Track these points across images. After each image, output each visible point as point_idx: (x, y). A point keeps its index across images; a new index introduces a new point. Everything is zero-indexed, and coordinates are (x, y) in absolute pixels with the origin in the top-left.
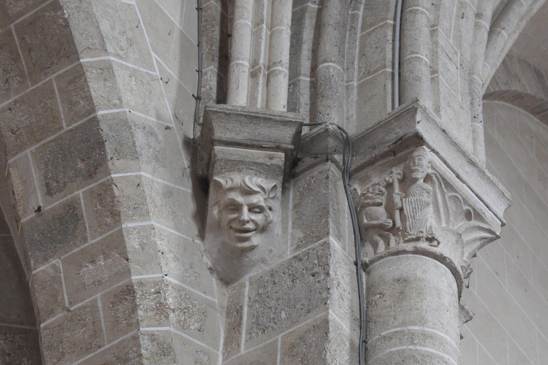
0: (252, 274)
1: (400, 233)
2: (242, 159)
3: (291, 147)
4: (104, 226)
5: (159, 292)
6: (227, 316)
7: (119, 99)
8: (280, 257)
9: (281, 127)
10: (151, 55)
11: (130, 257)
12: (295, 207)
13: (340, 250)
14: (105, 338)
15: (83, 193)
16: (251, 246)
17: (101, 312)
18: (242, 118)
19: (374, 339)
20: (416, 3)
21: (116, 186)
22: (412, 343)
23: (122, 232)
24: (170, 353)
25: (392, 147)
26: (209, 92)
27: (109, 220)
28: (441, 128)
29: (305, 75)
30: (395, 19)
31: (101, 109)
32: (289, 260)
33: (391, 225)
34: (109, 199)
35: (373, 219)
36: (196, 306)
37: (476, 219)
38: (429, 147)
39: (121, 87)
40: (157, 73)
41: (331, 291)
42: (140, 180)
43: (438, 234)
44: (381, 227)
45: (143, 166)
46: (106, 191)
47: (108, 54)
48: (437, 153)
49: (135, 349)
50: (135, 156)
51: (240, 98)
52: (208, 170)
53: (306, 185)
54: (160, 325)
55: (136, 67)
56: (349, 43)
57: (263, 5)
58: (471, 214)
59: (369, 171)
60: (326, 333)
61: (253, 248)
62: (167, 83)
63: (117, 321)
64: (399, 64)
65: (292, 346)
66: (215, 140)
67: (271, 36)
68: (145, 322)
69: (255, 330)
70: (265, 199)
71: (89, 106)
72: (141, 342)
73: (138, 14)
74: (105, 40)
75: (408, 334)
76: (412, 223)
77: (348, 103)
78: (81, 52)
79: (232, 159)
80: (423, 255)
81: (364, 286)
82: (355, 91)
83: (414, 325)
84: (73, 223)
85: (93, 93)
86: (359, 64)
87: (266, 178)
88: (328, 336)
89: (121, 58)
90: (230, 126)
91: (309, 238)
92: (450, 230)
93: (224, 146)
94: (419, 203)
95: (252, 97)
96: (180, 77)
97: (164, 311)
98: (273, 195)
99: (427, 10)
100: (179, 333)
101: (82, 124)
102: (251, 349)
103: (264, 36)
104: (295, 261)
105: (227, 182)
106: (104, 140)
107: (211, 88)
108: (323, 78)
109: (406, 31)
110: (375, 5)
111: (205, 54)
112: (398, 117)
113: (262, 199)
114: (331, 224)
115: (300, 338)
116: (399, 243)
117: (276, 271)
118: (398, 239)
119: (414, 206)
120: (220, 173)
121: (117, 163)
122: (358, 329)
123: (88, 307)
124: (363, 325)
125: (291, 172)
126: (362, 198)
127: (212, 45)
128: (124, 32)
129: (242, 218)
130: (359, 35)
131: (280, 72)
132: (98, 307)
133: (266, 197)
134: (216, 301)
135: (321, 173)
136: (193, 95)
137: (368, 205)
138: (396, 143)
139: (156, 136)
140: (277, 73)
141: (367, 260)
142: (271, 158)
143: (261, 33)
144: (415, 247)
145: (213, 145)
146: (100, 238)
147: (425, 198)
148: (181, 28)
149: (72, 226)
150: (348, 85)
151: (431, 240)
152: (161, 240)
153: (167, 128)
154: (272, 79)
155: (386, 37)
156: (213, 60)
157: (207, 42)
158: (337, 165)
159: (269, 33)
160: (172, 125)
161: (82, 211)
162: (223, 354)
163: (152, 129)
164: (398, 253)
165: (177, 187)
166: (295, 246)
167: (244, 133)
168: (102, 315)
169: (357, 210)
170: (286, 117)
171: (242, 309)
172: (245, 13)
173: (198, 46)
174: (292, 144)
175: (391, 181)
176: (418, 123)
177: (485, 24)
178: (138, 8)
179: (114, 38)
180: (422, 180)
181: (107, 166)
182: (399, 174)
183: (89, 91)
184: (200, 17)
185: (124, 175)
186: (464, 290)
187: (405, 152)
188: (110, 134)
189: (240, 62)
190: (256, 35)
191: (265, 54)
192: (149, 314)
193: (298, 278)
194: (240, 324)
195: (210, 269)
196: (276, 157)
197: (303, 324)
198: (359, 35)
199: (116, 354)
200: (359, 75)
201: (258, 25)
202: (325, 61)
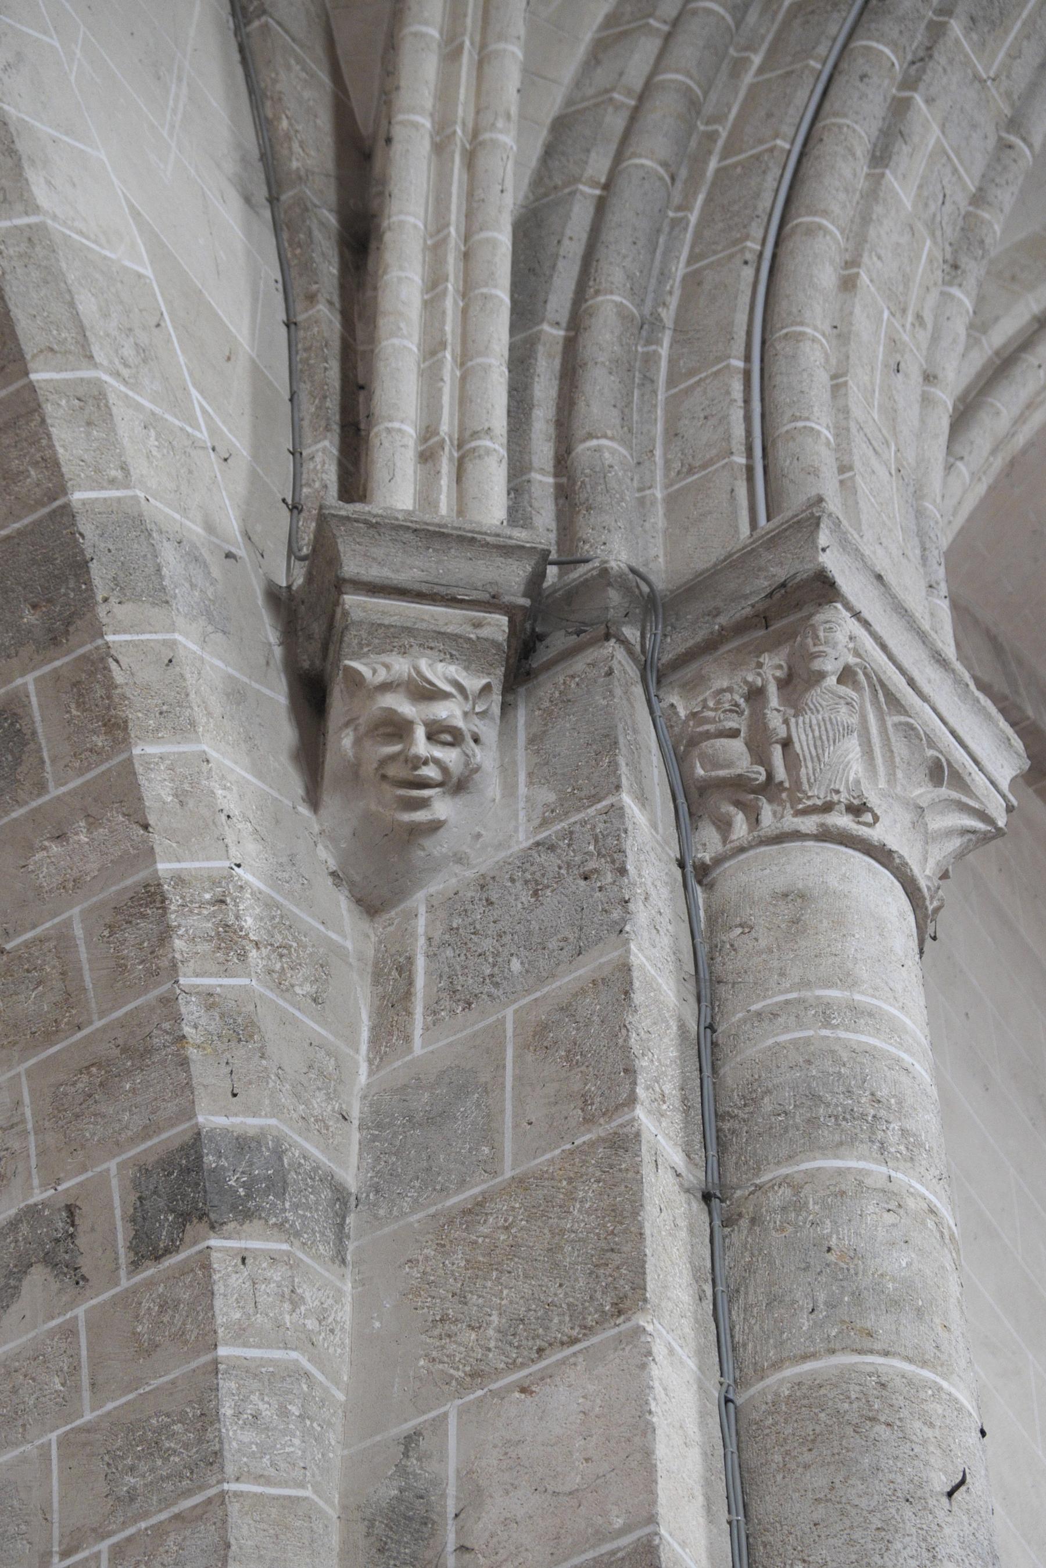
0: (432, 890)
1: (784, 795)
2: (409, 625)
3: (526, 602)
4: (88, 753)
5: (223, 902)
6: (376, 982)
7: (122, 468)
8: (500, 846)
9: (499, 561)
10: (189, 394)
11: (152, 820)
12: (531, 741)
13: (646, 825)
14: (93, 1005)
15: (36, 680)
16: (432, 821)
17: (82, 949)
18: (408, 536)
19: (734, 1020)
20: (798, 320)
21: (117, 661)
22: (827, 1024)
23: (132, 763)
24: (251, 1036)
25: (760, 607)
26: (322, 493)
27: (99, 741)
28: (873, 571)
29: (542, 471)
30: (748, 358)
31: (80, 488)
32: (523, 850)
33: (763, 778)
34: (100, 692)
35: (717, 766)
36: (305, 947)
37: (950, 786)
38: (848, 607)
39: (126, 441)
40: (203, 435)
41: (631, 906)
42: (173, 650)
43: (873, 800)
44: (739, 783)
45: (180, 621)
46: (91, 674)
47: (96, 366)
48: (866, 624)
49: (166, 1026)
50: (161, 597)
51: (399, 487)
52: (325, 657)
53: (557, 694)
54: (226, 973)
55: (157, 410)
56: (640, 410)
57: (444, 312)
58: (939, 772)
59: (706, 665)
60: (626, 993)
61: (435, 826)
62: (226, 460)
63: (121, 967)
64: (764, 449)
65: (543, 1028)
66: (344, 580)
67: (463, 379)
68: (191, 964)
69: (447, 1003)
70: (466, 714)
71: (50, 480)
72: (183, 1010)
73: (160, 299)
74: (88, 334)
75: (817, 1006)
76: (814, 770)
77: (645, 532)
78: (34, 356)
79: (386, 622)
80: (841, 843)
81: (702, 913)
82: (660, 509)
83: (829, 987)
84: (11, 752)
85: (60, 450)
86: (665, 454)
87: (466, 668)
88: (630, 998)
89: (125, 382)
90: (379, 552)
91: (574, 797)
92: (898, 798)
93: (367, 596)
94: (829, 726)
95: (426, 496)
96: (255, 457)
97: (236, 943)
98: (484, 708)
99: (824, 335)
100: (271, 995)
101: (33, 523)
102: (440, 1044)
103: (447, 377)
104: (539, 852)
105: (375, 672)
106: (88, 557)
107: (326, 487)
108: (587, 471)
109: (779, 378)
110: (698, 331)
111: (308, 418)
112: (772, 541)
113: (458, 713)
114: (624, 769)
115: (562, 1009)
116: (782, 817)
117: (493, 878)
118: (779, 809)
119: (817, 733)
120: (357, 656)
121: (117, 609)
122: (692, 1000)
123: (48, 939)
124: (706, 993)
125: (522, 664)
126: (691, 723)
127: (325, 397)
128: (130, 330)
129: (414, 750)
130: (661, 396)
131: (488, 452)
132: (74, 938)
133: (468, 707)
134: (349, 945)
135: (593, 665)
136: (284, 500)
137: (708, 736)
138: (770, 595)
139: (206, 566)
140: (482, 452)
141: (707, 858)
142: (477, 625)
143: (440, 369)
144: (822, 825)
145: (340, 593)
146: (78, 782)
147: (844, 715)
148: (254, 356)
149: (10, 758)
150: (644, 497)
151: (857, 810)
152: (225, 788)
153: (229, 555)
154: (469, 466)
155: (728, 393)
156: (327, 428)
157: (311, 393)
158: (630, 652)
159: (458, 374)
160: (241, 552)
161: (34, 722)
162: (370, 1062)
163: (197, 548)
164: (780, 838)
165: (257, 686)
166: (537, 822)
167: (412, 568)
168: (84, 956)
169: (680, 748)
170: (510, 538)
171: (412, 964)
172: (402, 325)
173: (291, 400)
174: (525, 595)
175: (759, 683)
176: (824, 550)
177: (944, 397)
178: (159, 286)
179: (108, 335)
180: (834, 679)
181: (96, 617)
182: (780, 667)
183: (51, 446)
184: (293, 343)
185: (135, 637)
186: (928, 941)
187: (792, 618)
188: (103, 545)
189: (396, 425)
190: (430, 376)
191: (451, 415)
192: (199, 948)
193: (548, 887)
194: (408, 995)
195: (333, 874)
196: (489, 624)
197: (567, 979)
198: (661, 396)
199: (120, 1042)
200: (666, 475)
201: (433, 353)
202: (590, 436)
